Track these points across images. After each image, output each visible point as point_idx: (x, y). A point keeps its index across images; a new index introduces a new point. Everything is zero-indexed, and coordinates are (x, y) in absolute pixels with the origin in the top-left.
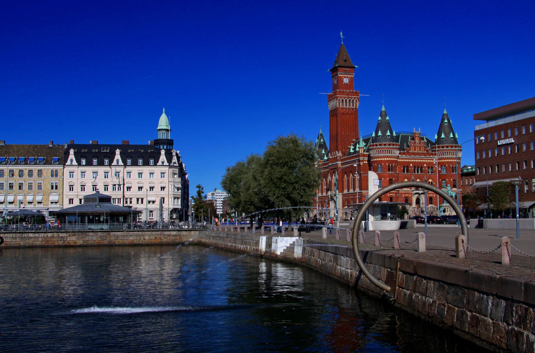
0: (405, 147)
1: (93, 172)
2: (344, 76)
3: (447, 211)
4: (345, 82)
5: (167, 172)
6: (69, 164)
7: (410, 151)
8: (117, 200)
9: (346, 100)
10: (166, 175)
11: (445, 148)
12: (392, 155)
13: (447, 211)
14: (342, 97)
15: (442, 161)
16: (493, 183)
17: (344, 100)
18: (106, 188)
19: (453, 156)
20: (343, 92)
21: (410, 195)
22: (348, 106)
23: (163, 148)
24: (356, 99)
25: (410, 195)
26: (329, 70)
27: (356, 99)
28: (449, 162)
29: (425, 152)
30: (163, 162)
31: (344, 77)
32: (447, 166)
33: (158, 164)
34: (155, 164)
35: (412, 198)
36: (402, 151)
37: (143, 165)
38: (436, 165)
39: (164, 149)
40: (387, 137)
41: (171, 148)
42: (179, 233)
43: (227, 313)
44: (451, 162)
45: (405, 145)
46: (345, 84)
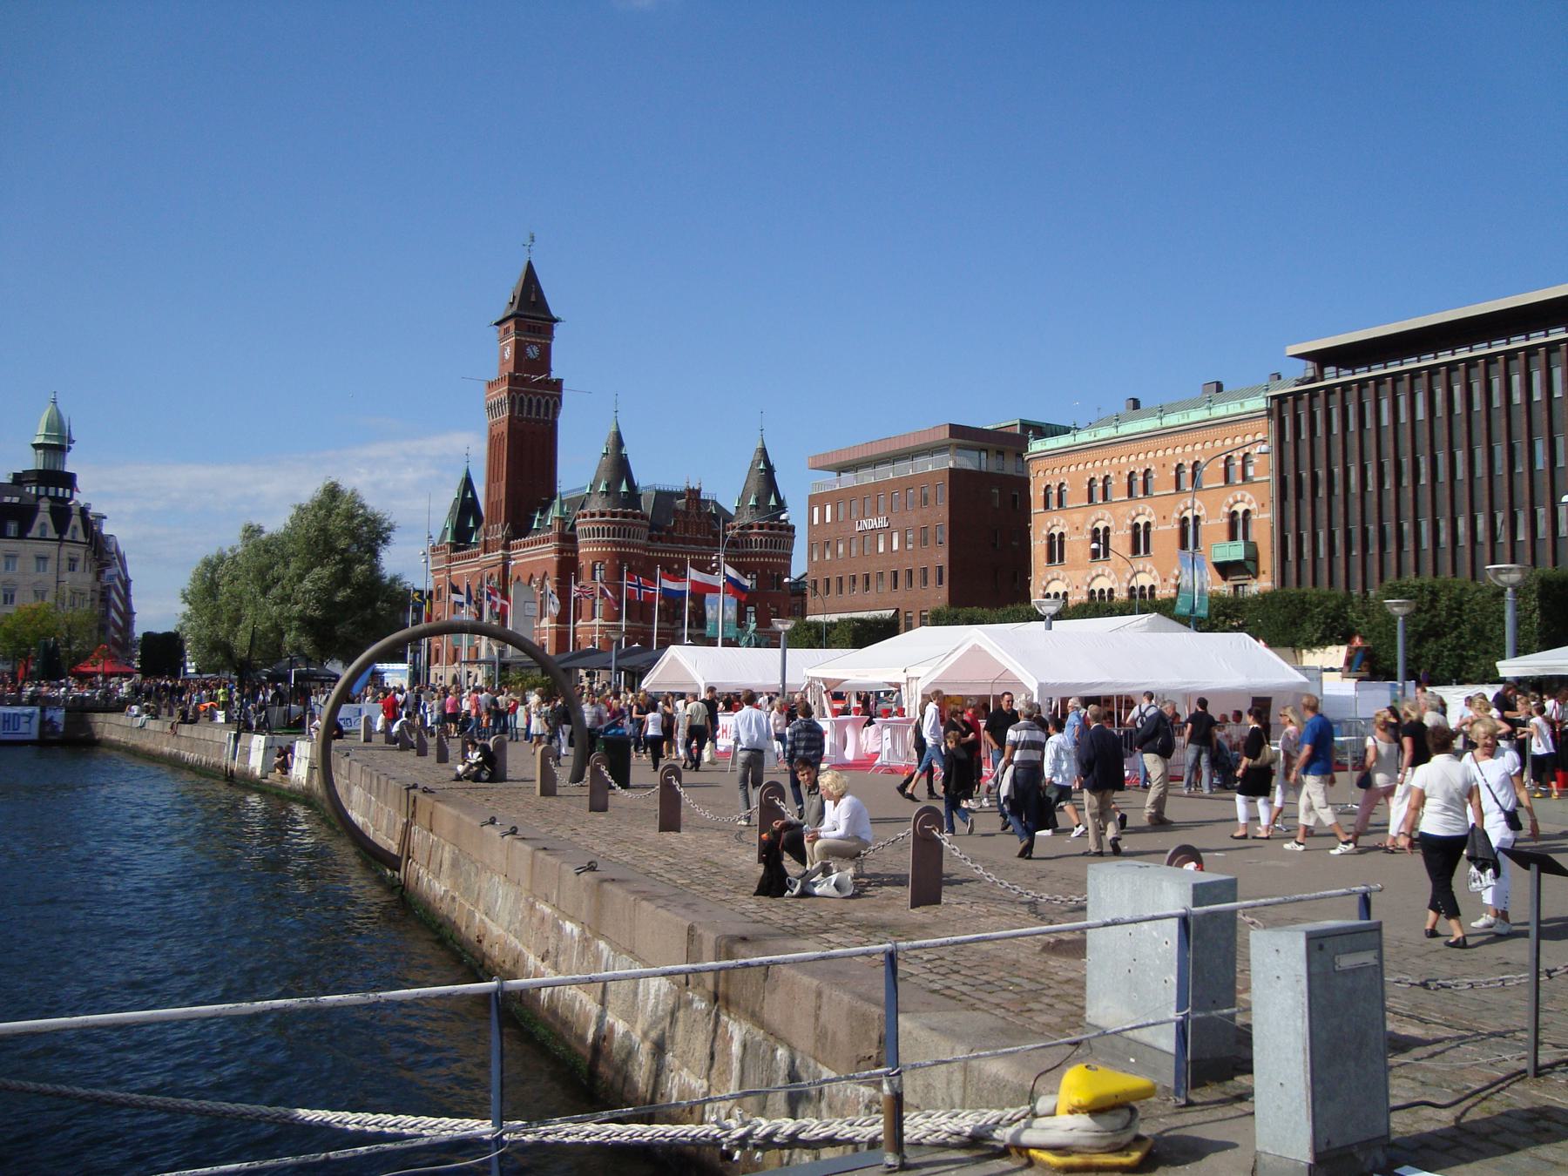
1: (7, 556)
4: (531, 355)
5: (82, 557)
6: (38, 536)
7: (675, 534)
8: (464, 657)
9: (547, 402)
10: (80, 565)
12: (635, 540)
14: (521, 391)
16: (839, 619)
17: (526, 400)
19: (773, 550)
20: (525, 379)
22: (525, 412)
23: (47, 495)
28: (761, 563)
29: (711, 537)
30: (43, 533)
33: (29, 535)
34: (22, 535)
36: (655, 533)
37: (17, 538)
39: (50, 498)
41: (68, 495)
43: (596, 975)
44: (768, 565)
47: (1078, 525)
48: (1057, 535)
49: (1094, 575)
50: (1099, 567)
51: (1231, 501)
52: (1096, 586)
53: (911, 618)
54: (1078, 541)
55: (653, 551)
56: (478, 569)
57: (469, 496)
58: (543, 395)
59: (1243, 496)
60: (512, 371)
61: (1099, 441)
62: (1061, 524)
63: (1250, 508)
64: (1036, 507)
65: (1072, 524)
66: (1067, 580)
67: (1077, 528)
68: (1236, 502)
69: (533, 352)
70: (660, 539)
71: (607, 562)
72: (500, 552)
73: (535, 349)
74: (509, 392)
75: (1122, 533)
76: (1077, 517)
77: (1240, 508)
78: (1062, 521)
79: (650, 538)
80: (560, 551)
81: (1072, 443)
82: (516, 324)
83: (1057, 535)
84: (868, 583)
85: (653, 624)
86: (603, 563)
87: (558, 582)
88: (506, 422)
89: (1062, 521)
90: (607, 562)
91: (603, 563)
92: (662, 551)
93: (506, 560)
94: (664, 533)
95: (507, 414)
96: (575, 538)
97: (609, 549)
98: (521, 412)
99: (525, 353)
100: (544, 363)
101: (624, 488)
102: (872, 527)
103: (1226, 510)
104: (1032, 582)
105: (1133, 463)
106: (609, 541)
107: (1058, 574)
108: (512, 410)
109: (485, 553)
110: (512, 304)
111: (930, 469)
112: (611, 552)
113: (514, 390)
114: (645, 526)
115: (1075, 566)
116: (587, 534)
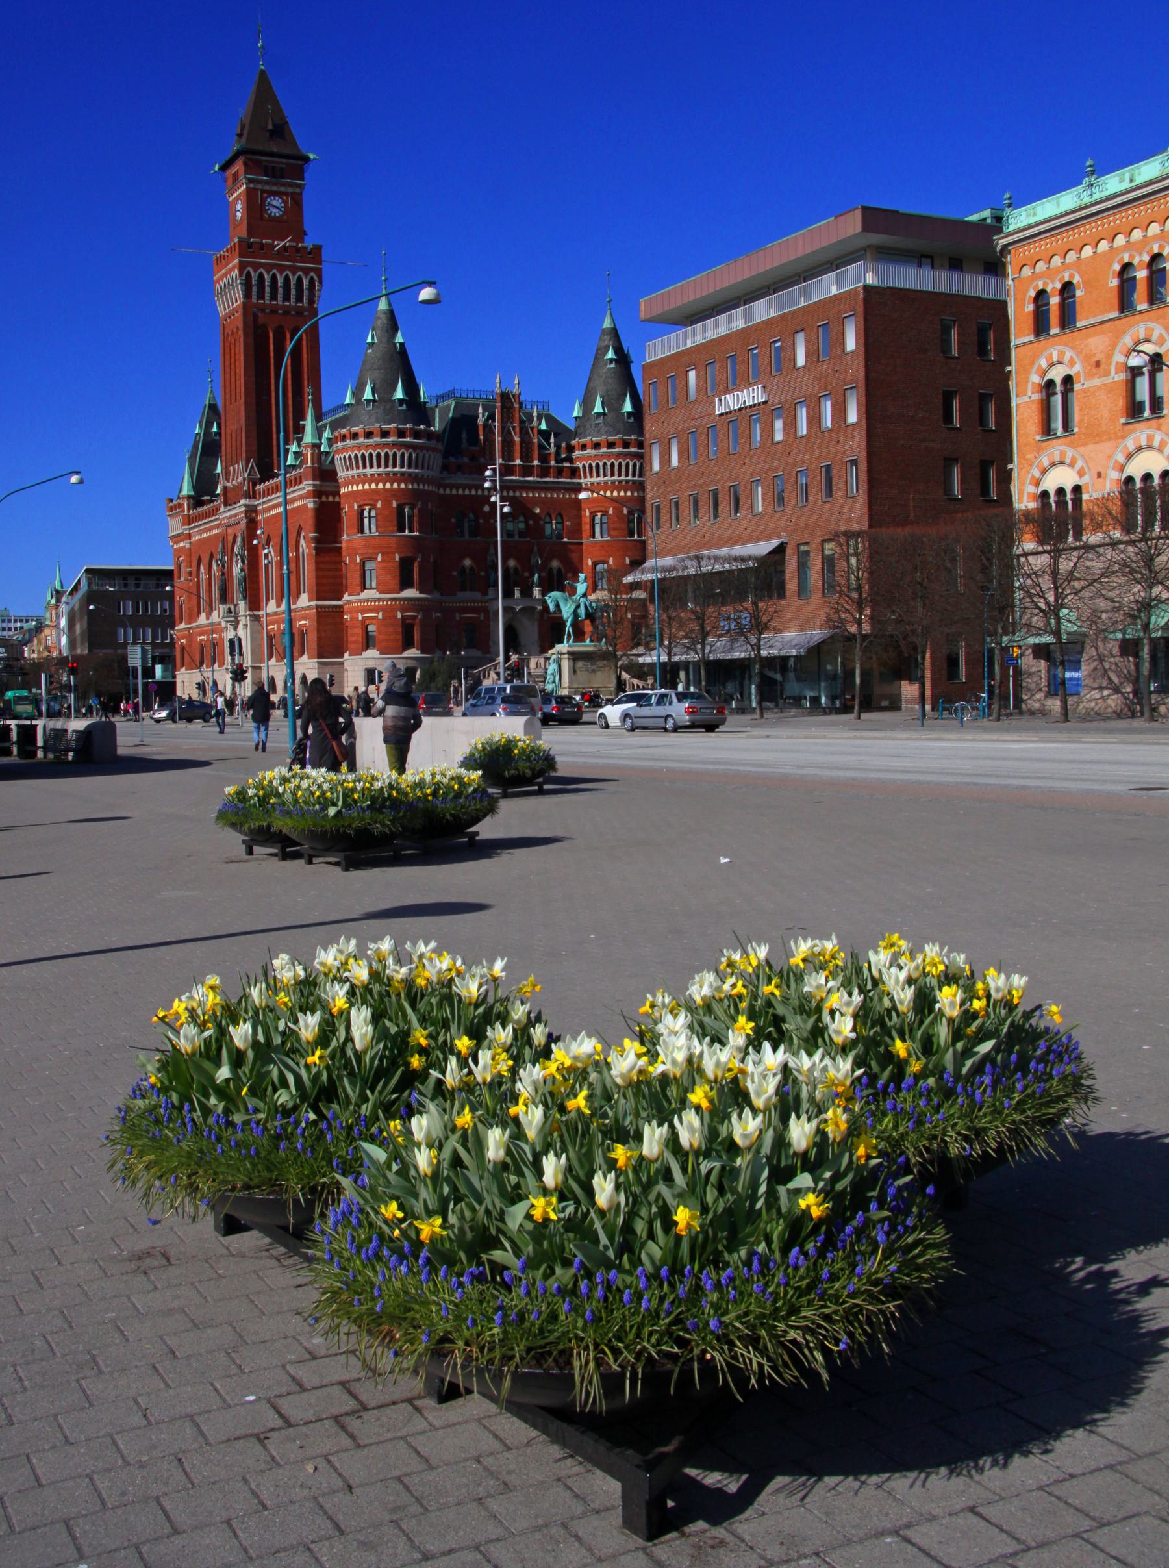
0: (465, 445)
2: (267, 188)
3: (802, 590)
4: (275, 212)
11: (604, 450)
13: (802, 590)
15: (360, 487)
18: (266, 556)
20: (262, 246)
21: (482, 617)
24: (312, 274)
25: (482, 617)
26: (217, 168)
27: (312, 274)
31: (266, 191)
32: (611, 511)
35: (489, 626)
38: (502, 514)
40: (393, 407)
42: (355, 642)
45: (464, 436)
46: (272, 219)
47: (1099, 357)
48: (1058, 380)
49: (1131, 447)
50: (1141, 433)
51: (1043, 363)
52: (1136, 469)
53: (807, 553)
54: (1098, 388)
55: (452, 486)
56: (219, 530)
57: (215, 429)
58: (294, 270)
59: (1061, 354)
60: (245, 235)
61: (1139, 187)
62: (1066, 360)
63: (1072, 373)
64: (1020, 336)
65: (1086, 359)
66: (1080, 464)
67: (1098, 364)
68: (1051, 365)
69: (276, 206)
70: (460, 468)
71: (379, 505)
72: (242, 502)
73: (277, 202)
74: (242, 266)
75: (1026, 399)
76: (1097, 343)
77: (1057, 374)
78: (1068, 354)
79: (445, 468)
80: (317, 493)
81: (1087, 200)
82: (245, 164)
83: (1058, 380)
84: (696, 504)
85: (502, 541)
86: (373, 507)
87: (317, 540)
88: (241, 311)
89: (1068, 354)
90: (379, 505)
91: (373, 507)
92: (464, 487)
93: (251, 511)
94: (466, 460)
95: (241, 300)
96: (334, 473)
97: (395, 486)
98: (261, 295)
99: (262, 208)
100: (292, 223)
101: (399, 394)
102: (740, 405)
103: (1035, 379)
104: (1015, 474)
105: (1156, 238)
106: (403, 474)
107: (1063, 454)
108: (247, 294)
109: (226, 505)
110: (240, 135)
111: (803, 304)
112: (406, 489)
113: (249, 264)
114: (434, 450)
115: (1095, 435)
116: (350, 464)
